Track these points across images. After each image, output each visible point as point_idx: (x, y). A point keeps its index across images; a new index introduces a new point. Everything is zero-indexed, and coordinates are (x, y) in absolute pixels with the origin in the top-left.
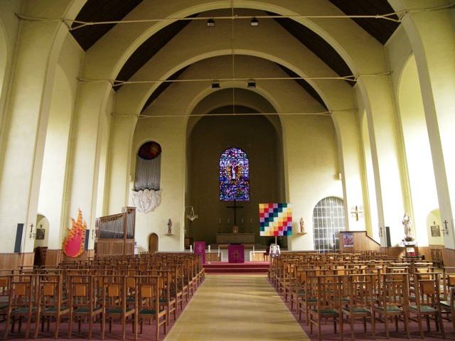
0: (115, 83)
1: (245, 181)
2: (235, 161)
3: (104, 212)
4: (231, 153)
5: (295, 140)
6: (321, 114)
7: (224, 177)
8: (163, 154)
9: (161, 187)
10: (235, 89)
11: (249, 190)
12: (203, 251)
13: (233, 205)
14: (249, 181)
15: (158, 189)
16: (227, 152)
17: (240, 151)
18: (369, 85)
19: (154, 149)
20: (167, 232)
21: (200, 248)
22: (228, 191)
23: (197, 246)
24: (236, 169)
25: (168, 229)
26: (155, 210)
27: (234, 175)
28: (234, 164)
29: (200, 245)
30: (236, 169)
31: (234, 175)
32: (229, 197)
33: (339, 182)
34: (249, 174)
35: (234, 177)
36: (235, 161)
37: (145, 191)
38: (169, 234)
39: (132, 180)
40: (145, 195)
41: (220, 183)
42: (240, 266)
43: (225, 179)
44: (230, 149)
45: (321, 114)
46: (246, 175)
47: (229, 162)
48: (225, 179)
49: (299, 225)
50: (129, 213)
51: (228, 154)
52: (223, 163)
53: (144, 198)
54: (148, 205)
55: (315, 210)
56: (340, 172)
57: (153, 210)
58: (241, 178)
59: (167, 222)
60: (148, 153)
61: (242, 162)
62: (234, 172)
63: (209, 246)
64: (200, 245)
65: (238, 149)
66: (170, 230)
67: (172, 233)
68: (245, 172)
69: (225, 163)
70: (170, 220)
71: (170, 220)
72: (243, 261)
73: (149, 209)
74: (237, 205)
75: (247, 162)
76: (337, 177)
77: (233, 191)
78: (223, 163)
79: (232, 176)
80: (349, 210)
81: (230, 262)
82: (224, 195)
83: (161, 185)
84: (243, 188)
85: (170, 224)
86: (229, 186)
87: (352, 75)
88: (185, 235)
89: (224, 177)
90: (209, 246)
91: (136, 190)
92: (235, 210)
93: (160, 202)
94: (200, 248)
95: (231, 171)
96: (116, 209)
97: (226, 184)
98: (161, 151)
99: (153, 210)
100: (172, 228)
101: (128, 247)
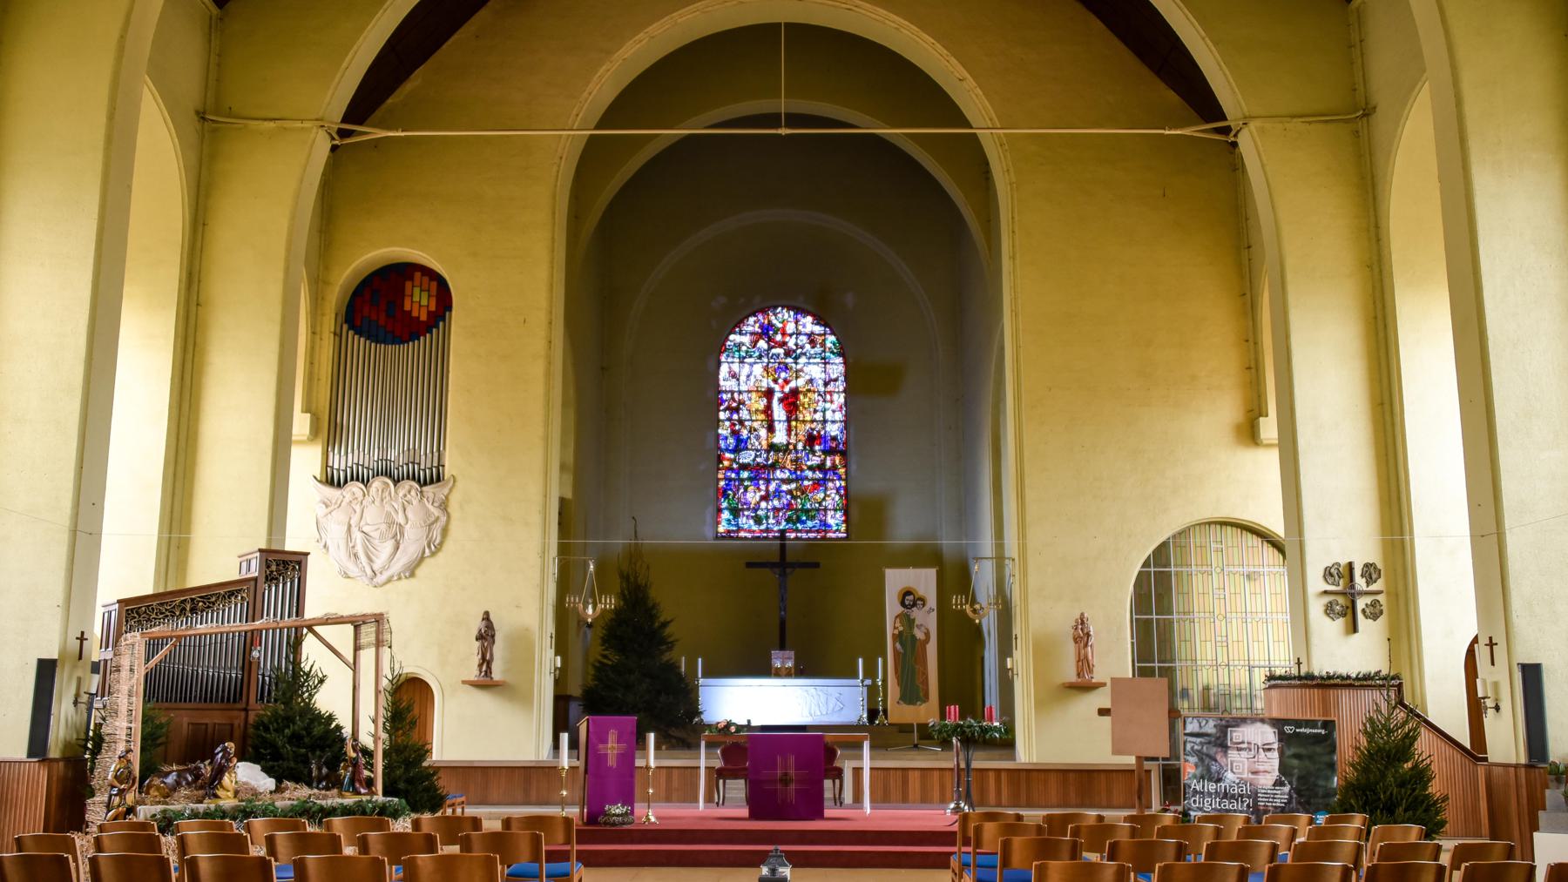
0: (343, 134)
1: (828, 452)
2: (786, 368)
3: (156, 583)
4: (766, 331)
5: (1058, 277)
6: (1187, 132)
7: (735, 434)
8: (457, 316)
9: (448, 471)
10: (790, 27)
11: (847, 494)
12: (627, 759)
13: (776, 559)
14: (844, 454)
15: (437, 479)
16: (752, 324)
17: (808, 324)
18: (1285, 174)
19: (419, 301)
20: (473, 673)
21: (612, 748)
22: (752, 497)
23: (597, 737)
24: (792, 401)
25: (477, 659)
26: (419, 572)
27: (780, 428)
28: (781, 376)
29: (612, 736)
30: (792, 401)
31: (780, 428)
32: (758, 521)
33: (1267, 463)
34: (846, 423)
35: (780, 437)
36: (786, 368)
37: (377, 484)
38: (486, 682)
39: (315, 431)
40: (376, 505)
41: (720, 459)
42: (803, 837)
43: (740, 445)
44: (764, 311)
45: (1187, 132)
46: (833, 430)
47: (758, 369)
48: (740, 445)
49: (1070, 649)
50: (270, 579)
51: (757, 337)
52: (734, 376)
53: (373, 517)
54: (389, 546)
55: (1142, 580)
56: (1262, 407)
57: (411, 571)
58: (811, 440)
59: (477, 625)
60: (391, 312)
61: (815, 371)
62: (779, 413)
63: (652, 737)
64: (612, 736)
65: (800, 311)
66: (486, 662)
67: (497, 675)
68: (830, 414)
69: (742, 374)
70: (486, 617)
71: (486, 617)
72: (818, 813)
73: (397, 567)
74: (790, 558)
75: (837, 368)
76: (1249, 433)
77: (778, 493)
78: (734, 376)
79: (771, 429)
80: (1316, 583)
81: (754, 815)
82: (736, 512)
83: (447, 462)
84: (819, 484)
85: (487, 635)
86: (759, 472)
87: (1225, 119)
88: (560, 682)
89: (735, 434)
90: (652, 737)
91: (330, 481)
92: (783, 575)
93: (445, 532)
94: (612, 748)
95: (768, 410)
96: (220, 557)
97: (744, 467)
98: (450, 308)
99: (411, 571)
100: (499, 650)
101: (948, 794)
